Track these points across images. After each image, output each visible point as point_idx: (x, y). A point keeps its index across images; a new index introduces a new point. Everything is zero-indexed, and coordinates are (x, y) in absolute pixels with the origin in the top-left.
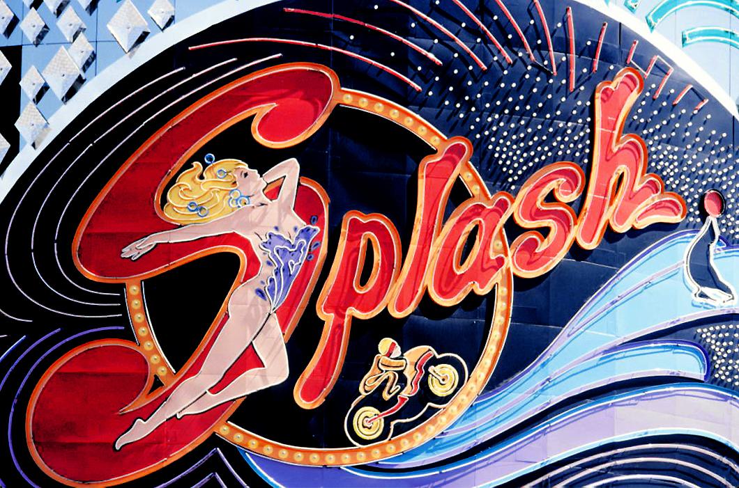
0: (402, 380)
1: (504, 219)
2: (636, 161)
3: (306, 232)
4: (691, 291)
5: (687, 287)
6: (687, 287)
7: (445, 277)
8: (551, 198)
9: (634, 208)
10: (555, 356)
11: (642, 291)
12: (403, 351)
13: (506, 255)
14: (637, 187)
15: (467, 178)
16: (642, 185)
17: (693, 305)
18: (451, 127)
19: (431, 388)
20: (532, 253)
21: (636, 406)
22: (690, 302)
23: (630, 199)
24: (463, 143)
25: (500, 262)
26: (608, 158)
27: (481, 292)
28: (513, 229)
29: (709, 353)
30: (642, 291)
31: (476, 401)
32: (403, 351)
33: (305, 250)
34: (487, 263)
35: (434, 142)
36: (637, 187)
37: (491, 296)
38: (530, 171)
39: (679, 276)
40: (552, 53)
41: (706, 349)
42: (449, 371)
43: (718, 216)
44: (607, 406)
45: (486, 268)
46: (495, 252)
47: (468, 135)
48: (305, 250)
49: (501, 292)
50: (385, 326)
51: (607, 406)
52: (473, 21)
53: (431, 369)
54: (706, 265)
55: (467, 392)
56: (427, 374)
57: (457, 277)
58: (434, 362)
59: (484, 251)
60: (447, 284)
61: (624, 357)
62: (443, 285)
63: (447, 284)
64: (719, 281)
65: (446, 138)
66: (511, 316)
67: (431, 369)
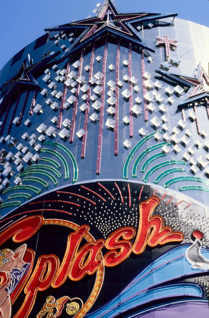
0: (55, 311)
1: (101, 247)
2: (159, 224)
3: (25, 266)
4: (191, 265)
5: (189, 264)
6: (189, 264)
7: (76, 272)
8: (121, 238)
9: (158, 239)
10: (124, 294)
11: (165, 266)
12: (56, 300)
13: (102, 260)
14: (160, 231)
15: (87, 238)
16: (162, 231)
17: (192, 269)
18: (81, 222)
19: (68, 313)
20: (113, 258)
21: (166, 310)
22: (191, 269)
23: (157, 235)
24: (133, 231)
25: (99, 262)
26: (146, 224)
27: (90, 273)
28: (105, 251)
29: (203, 287)
30: (165, 266)
31: (87, 314)
32: (56, 300)
33: (24, 272)
34: (94, 264)
35: (75, 228)
36: (160, 231)
37: (95, 275)
38: (112, 232)
39: (184, 259)
40: (44, 201)
41: (202, 285)
42: (76, 305)
43: (201, 238)
44: (150, 311)
45: (92, 265)
46: (97, 259)
47: (89, 224)
48: (24, 272)
49: (98, 273)
50: (51, 292)
51: (150, 311)
52: (103, 189)
53: (68, 305)
54: (197, 255)
55: (83, 312)
56: (66, 306)
57: (81, 271)
58: (69, 302)
59: (93, 260)
60: (77, 274)
61: (158, 291)
62: (75, 275)
63: (77, 274)
64: (205, 261)
65: (79, 226)
66: (169, 304)
67: (68, 305)
